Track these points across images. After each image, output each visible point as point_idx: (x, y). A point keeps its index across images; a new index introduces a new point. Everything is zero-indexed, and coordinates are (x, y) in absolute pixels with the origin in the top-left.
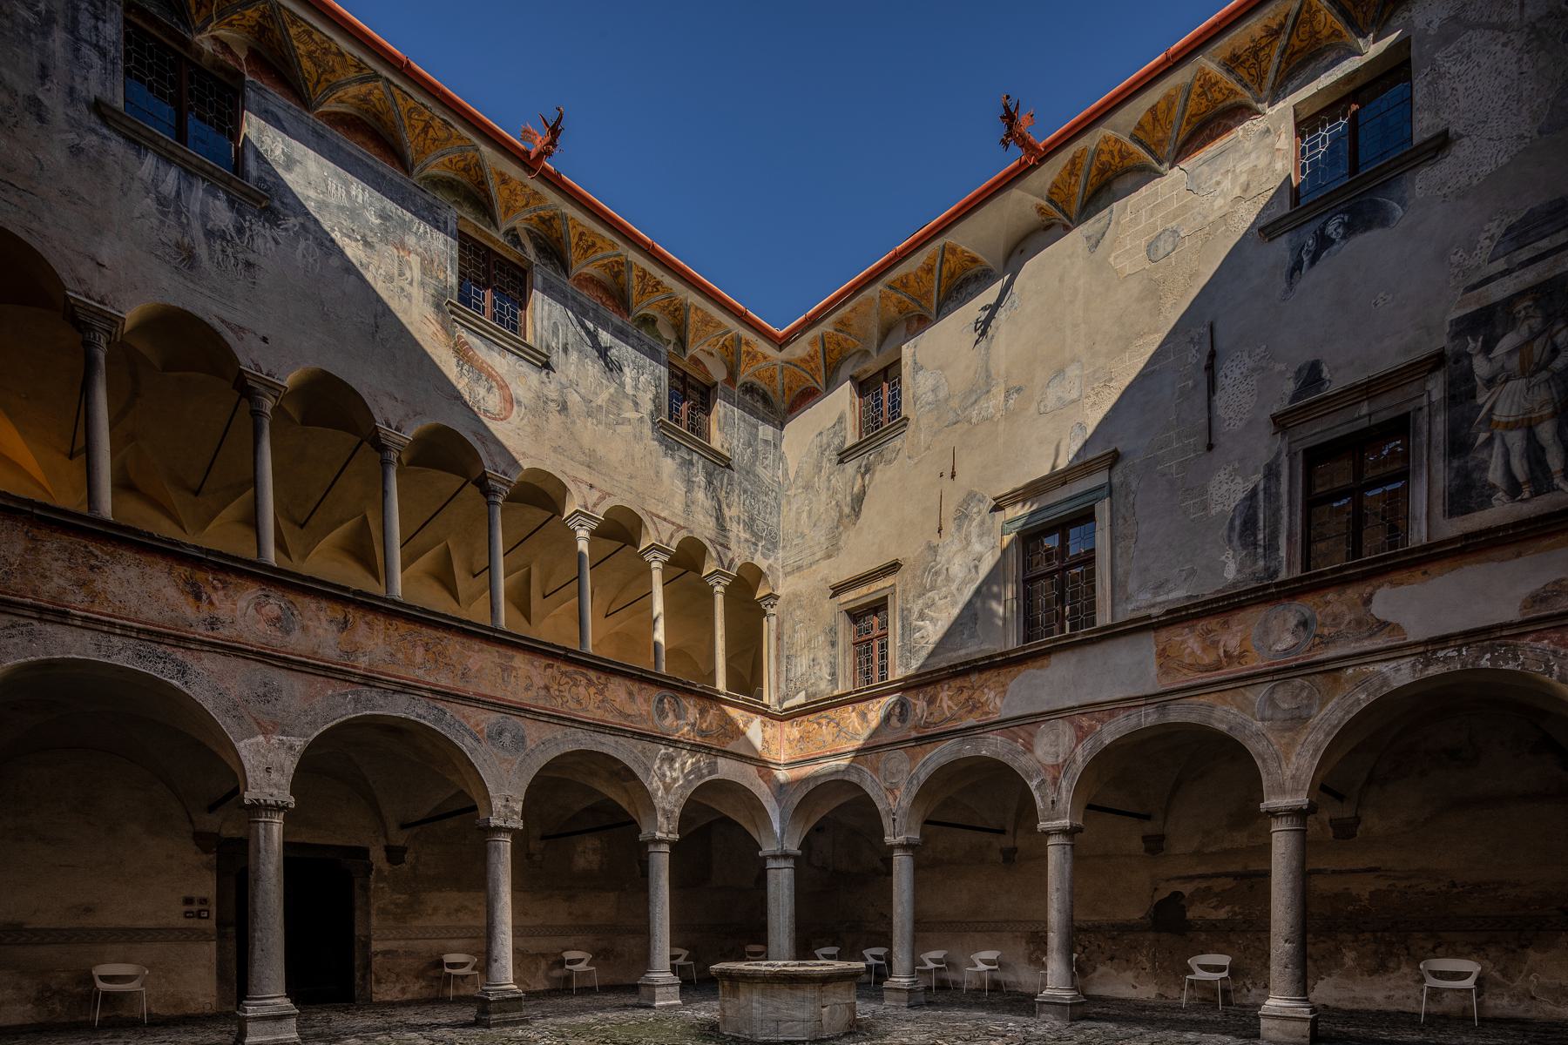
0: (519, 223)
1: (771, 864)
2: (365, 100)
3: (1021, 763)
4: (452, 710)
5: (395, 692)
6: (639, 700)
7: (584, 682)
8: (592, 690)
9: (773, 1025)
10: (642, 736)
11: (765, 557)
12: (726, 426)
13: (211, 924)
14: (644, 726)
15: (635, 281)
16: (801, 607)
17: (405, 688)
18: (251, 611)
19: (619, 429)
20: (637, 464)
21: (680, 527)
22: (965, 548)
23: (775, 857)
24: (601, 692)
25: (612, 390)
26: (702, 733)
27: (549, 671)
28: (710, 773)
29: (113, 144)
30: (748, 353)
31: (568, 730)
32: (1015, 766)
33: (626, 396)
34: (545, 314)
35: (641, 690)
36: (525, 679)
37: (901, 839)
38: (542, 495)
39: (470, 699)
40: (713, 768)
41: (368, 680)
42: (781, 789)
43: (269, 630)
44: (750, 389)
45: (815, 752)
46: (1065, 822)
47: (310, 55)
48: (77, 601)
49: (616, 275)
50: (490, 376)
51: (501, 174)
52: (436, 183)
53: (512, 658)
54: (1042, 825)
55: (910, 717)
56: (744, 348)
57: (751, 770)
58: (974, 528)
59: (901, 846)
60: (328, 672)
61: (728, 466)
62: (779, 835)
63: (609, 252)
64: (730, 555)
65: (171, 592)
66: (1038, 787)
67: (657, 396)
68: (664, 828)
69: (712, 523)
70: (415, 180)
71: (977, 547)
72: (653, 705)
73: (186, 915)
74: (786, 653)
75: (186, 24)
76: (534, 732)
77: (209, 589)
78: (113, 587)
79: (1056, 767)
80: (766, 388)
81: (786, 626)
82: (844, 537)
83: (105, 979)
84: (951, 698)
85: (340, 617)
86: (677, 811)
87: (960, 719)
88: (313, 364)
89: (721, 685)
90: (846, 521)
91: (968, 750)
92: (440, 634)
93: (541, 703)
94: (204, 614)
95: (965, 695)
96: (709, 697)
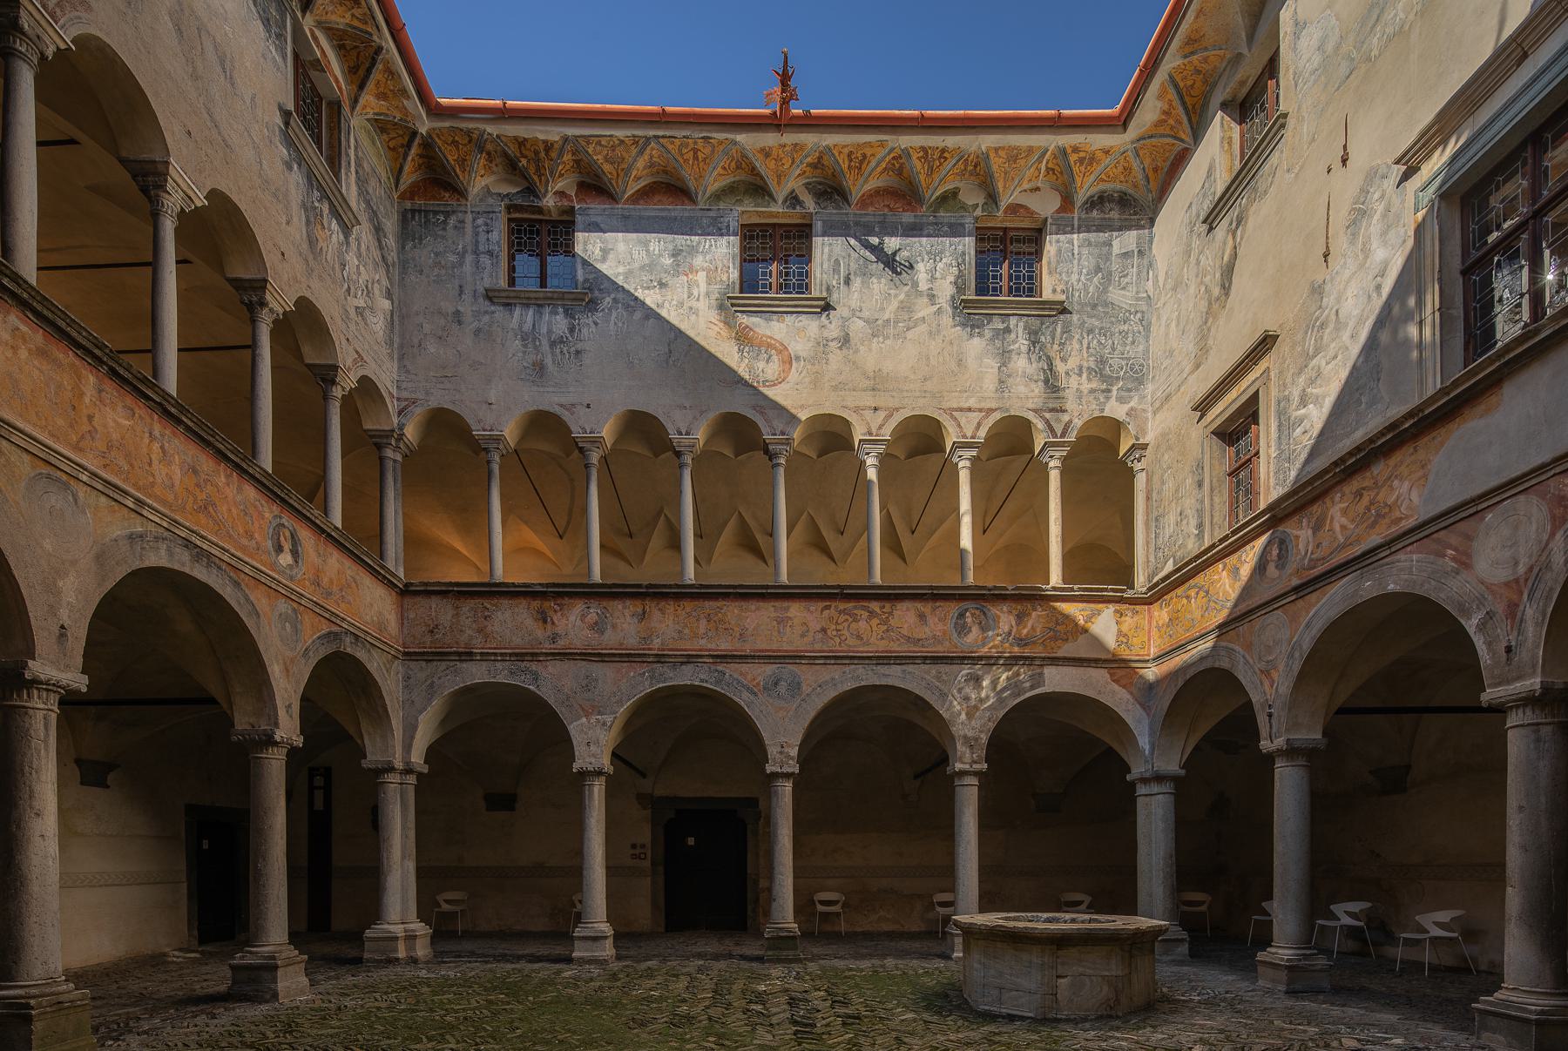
0: (794, 183)
1: (1141, 790)
2: (652, 165)
3: (1449, 591)
4: (731, 670)
6: (932, 620)
7: (865, 614)
8: (875, 622)
9: (995, 992)
10: (936, 660)
11: (1121, 400)
12: (1065, 263)
13: (647, 864)
15: (918, 165)
16: (1170, 448)
17: (690, 659)
18: (578, 623)
19: (910, 334)
20: (933, 362)
21: (991, 411)
23: (1145, 781)
24: (885, 622)
25: (902, 297)
26: (1021, 642)
28: (1032, 688)
30: (1081, 160)
31: (847, 669)
32: (1440, 597)
33: (920, 294)
34: (825, 257)
36: (801, 625)
37: (1280, 742)
38: (832, 436)
39: (746, 657)
40: (1038, 680)
41: (660, 658)
42: (1149, 690)
43: (589, 633)
44: (1098, 201)
45: (1184, 636)
46: (1534, 683)
47: (606, 160)
48: (478, 645)
49: (900, 172)
50: (769, 346)
51: (762, 150)
52: (718, 196)
53: (787, 609)
54: (1489, 695)
56: (1073, 158)
57: (1100, 675)
58: (1375, 225)
59: (1281, 753)
60: (629, 658)
61: (1064, 311)
62: (1152, 752)
63: (882, 153)
64: (1066, 418)
65: (529, 622)
66: (1482, 627)
67: (960, 275)
68: (967, 759)
71: (1379, 254)
72: (950, 625)
73: (634, 856)
74: (1155, 513)
75: (537, 196)
76: (809, 676)
79: (1515, 584)
80: (1123, 187)
81: (1156, 479)
82: (1213, 330)
83: (822, 903)
84: (1345, 512)
85: (640, 610)
86: (984, 738)
87: (1358, 541)
88: (621, 409)
89: (1055, 577)
90: (1215, 306)
92: (720, 603)
93: (818, 646)
95: (1365, 500)
96: (1030, 598)
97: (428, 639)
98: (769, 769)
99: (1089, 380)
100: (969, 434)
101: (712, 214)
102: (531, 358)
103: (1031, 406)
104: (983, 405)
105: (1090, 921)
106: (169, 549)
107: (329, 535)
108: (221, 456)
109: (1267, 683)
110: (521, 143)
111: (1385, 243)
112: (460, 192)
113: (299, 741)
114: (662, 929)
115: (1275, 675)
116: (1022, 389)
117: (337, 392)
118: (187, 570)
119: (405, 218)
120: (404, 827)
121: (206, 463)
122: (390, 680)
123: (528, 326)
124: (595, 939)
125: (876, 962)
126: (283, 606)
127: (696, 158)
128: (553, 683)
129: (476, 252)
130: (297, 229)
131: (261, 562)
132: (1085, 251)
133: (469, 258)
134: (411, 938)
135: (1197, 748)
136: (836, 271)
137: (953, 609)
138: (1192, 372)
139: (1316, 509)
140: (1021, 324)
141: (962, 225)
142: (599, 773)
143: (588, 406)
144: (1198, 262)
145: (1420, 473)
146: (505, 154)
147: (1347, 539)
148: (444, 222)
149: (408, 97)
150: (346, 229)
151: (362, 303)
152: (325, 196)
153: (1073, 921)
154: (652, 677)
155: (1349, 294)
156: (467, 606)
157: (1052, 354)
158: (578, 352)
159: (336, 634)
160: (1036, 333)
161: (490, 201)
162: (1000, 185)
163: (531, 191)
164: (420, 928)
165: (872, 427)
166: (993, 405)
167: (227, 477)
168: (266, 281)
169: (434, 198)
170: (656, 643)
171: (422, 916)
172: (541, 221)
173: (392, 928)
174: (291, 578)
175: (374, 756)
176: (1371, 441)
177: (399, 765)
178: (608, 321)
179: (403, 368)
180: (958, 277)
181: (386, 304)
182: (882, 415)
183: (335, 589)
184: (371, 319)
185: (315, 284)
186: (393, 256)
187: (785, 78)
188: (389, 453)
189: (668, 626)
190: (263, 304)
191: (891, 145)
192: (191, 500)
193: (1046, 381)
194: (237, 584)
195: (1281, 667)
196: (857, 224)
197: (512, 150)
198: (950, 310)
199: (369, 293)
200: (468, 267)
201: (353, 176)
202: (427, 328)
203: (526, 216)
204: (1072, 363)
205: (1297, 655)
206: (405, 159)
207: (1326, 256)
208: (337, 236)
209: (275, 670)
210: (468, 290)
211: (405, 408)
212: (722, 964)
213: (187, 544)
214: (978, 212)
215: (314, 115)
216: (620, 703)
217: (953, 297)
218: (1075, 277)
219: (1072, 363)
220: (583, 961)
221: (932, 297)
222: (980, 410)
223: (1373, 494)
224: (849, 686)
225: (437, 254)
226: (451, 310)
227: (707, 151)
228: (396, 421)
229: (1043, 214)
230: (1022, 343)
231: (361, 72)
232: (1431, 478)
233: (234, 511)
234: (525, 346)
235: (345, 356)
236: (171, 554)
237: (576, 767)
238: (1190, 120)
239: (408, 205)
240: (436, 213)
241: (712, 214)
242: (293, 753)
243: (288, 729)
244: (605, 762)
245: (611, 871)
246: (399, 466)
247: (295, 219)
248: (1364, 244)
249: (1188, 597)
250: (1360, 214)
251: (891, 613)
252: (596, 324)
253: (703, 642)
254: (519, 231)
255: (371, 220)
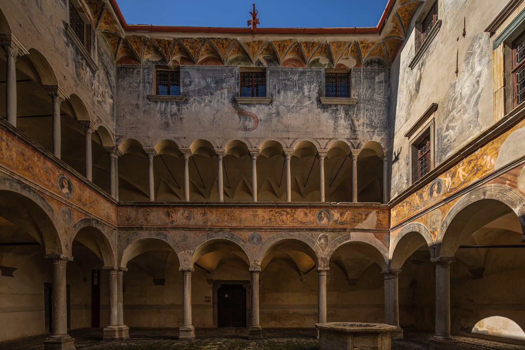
4: (237, 233)
5: (219, 231)
6: (309, 215)
7: (285, 213)
8: (289, 216)
10: (311, 230)
13: (211, 304)
14: (312, 225)
17: (221, 230)
18: (181, 216)
19: (301, 111)
22: (471, 74)
24: (292, 216)
27: (271, 213)
29: (152, 105)
30: (364, 47)
31: (278, 233)
32: (504, 200)
33: (305, 97)
34: (271, 83)
35: (310, 211)
40: (349, 237)
47: (191, 48)
50: (250, 116)
51: (247, 43)
52: (231, 62)
53: (257, 211)
55: (443, 189)
56: (361, 46)
58: (476, 58)
64: (358, 141)
65: (163, 216)
67: (320, 90)
69: (348, 131)
70: (226, 65)
71: (478, 69)
72: (316, 217)
73: (205, 301)
76: (265, 236)
77: (171, 213)
78: (151, 218)
82: (413, 107)
84: (464, 170)
85: (203, 212)
86: (328, 258)
87: (469, 181)
91: (474, 198)
93: (268, 225)
94: (170, 220)
95: (472, 165)
97: (127, 223)
98: (250, 269)
99: (367, 128)
100: (323, 148)
101: (229, 68)
102: (164, 120)
103: (346, 137)
104: (328, 137)
105: (367, 326)
106: (10, 183)
107: (85, 183)
108: (35, 150)
109: (433, 236)
110: (159, 41)
111: (480, 64)
112: (138, 61)
113: (71, 259)
114: (216, 327)
115: (436, 233)
116: (342, 131)
117: (90, 131)
118: (19, 192)
119: (118, 70)
120: (118, 291)
121: (28, 152)
122: (113, 239)
123: (163, 109)
124: (187, 331)
125: (289, 339)
126: (64, 208)
127: (223, 47)
128: (172, 238)
129: (144, 82)
130: (71, 68)
131: (54, 191)
132: (365, 81)
133: (141, 85)
134: (121, 331)
135: (406, 263)
136: (275, 88)
137: (317, 211)
138: (405, 123)
139: (453, 169)
140: (342, 108)
141: (321, 72)
142: (189, 271)
143: (185, 138)
144: (407, 82)
145: (495, 152)
146: (154, 46)
147: (465, 180)
148: (133, 72)
149: (117, 24)
150: (93, 72)
151: (100, 99)
152: (83, 58)
153: (361, 326)
154: (208, 236)
155: (466, 86)
156: (141, 210)
157: (353, 118)
158: (181, 118)
159: (88, 220)
160: (347, 111)
161: (149, 64)
162: (334, 56)
163: (164, 60)
164: (124, 327)
165: (292, 148)
166: (331, 137)
167: (38, 158)
168: (57, 86)
169: (129, 63)
170: (209, 224)
171: (125, 323)
172: (168, 72)
173: (113, 327)
174: (68, 198)
175: (107, 264)
176: (475, 141)
177: (116, 268)
178: (192, 107)
179: (117, 124)
180: (319, 90)
181: (111, 101)
182: (291, 141)
183: (88, 203)
184: (104, 105)
185: (79, 90)
186: (114, 84)
187: (254, 15)
188: (113, 155)
189: (214, 217)
190: (57, 95)
191: (294, 41)
192: (21, 165)
193: (351, 128)
194: (43, 199)
195: (439, 230)
196: (282, 71)
197: (156, 44)
198: (316, 103)
199: (103, 96)
200: (141, 88)
201: (96, 53)
202: (126, 110)
203: (162, 70)
204: (361, 121)
205: (445, 225)
206: (118, 48)
207: (457, 72)
208: (89, 74)
209: (60, 232)
210: (141, 96)
211: (118, 139)
212: (233, 341)
213: (19, 182)
214: (326, 67)
215: (78, 29)
216: (196, 246)
217: (317, 98)
218: (361, 90)
219: (361, 121)
220: (182, 339)
221: (310, 98)
222: (327, 139)
223: (475, 162)
224: (279, 239)
225: (130, 83)
226: (135, 103)
227: (227, 44)
228: (115, 143)
229: (350, 68)
230: (342, 115)
231: (98, 13)
232: (499, 153)
233: (41, 171)
234: (162, 116)
235: (93, 118)
236: (11, 186)
237: (180, 269)
238: (404, 30)
239: (120, 65)
240: (129, 68)
241: (229, 68)
242: (69, 263)
243: (66, 253)
244: (191, 267)
245: (193, 306)
246: (117, 161)
247: (70, 65)
248: (472, 66)
249: (403, 206)
250: (470, 54)
251: (294, 213)
252: (187, 108)
253: (226, 223)
254: (160, 75)
255: (104, 70)
